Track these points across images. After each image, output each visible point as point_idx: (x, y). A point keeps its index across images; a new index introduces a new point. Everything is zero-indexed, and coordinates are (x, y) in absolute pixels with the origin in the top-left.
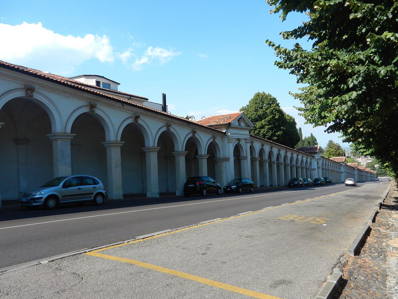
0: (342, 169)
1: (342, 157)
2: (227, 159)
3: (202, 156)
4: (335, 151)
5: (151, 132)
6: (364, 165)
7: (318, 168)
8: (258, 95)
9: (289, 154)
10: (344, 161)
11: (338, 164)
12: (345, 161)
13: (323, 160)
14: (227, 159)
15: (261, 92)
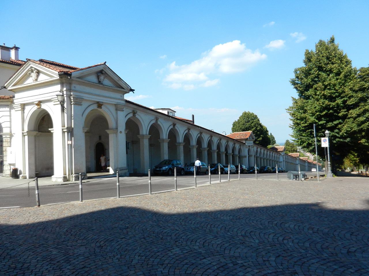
0: (297, 162)
1: (297, 153)
2: (245, 157)
3: (163, 140)
4: (291, 148)
5: (144, 125)
6: (312, 159)
7: (284, 161)
8: (245, 113)
9: (262, 151)
10: (298, 156)
11: (295, 158)
12: (299, 156)
13: (286, 156)
14: (245, 157)
15: (247, 112)
